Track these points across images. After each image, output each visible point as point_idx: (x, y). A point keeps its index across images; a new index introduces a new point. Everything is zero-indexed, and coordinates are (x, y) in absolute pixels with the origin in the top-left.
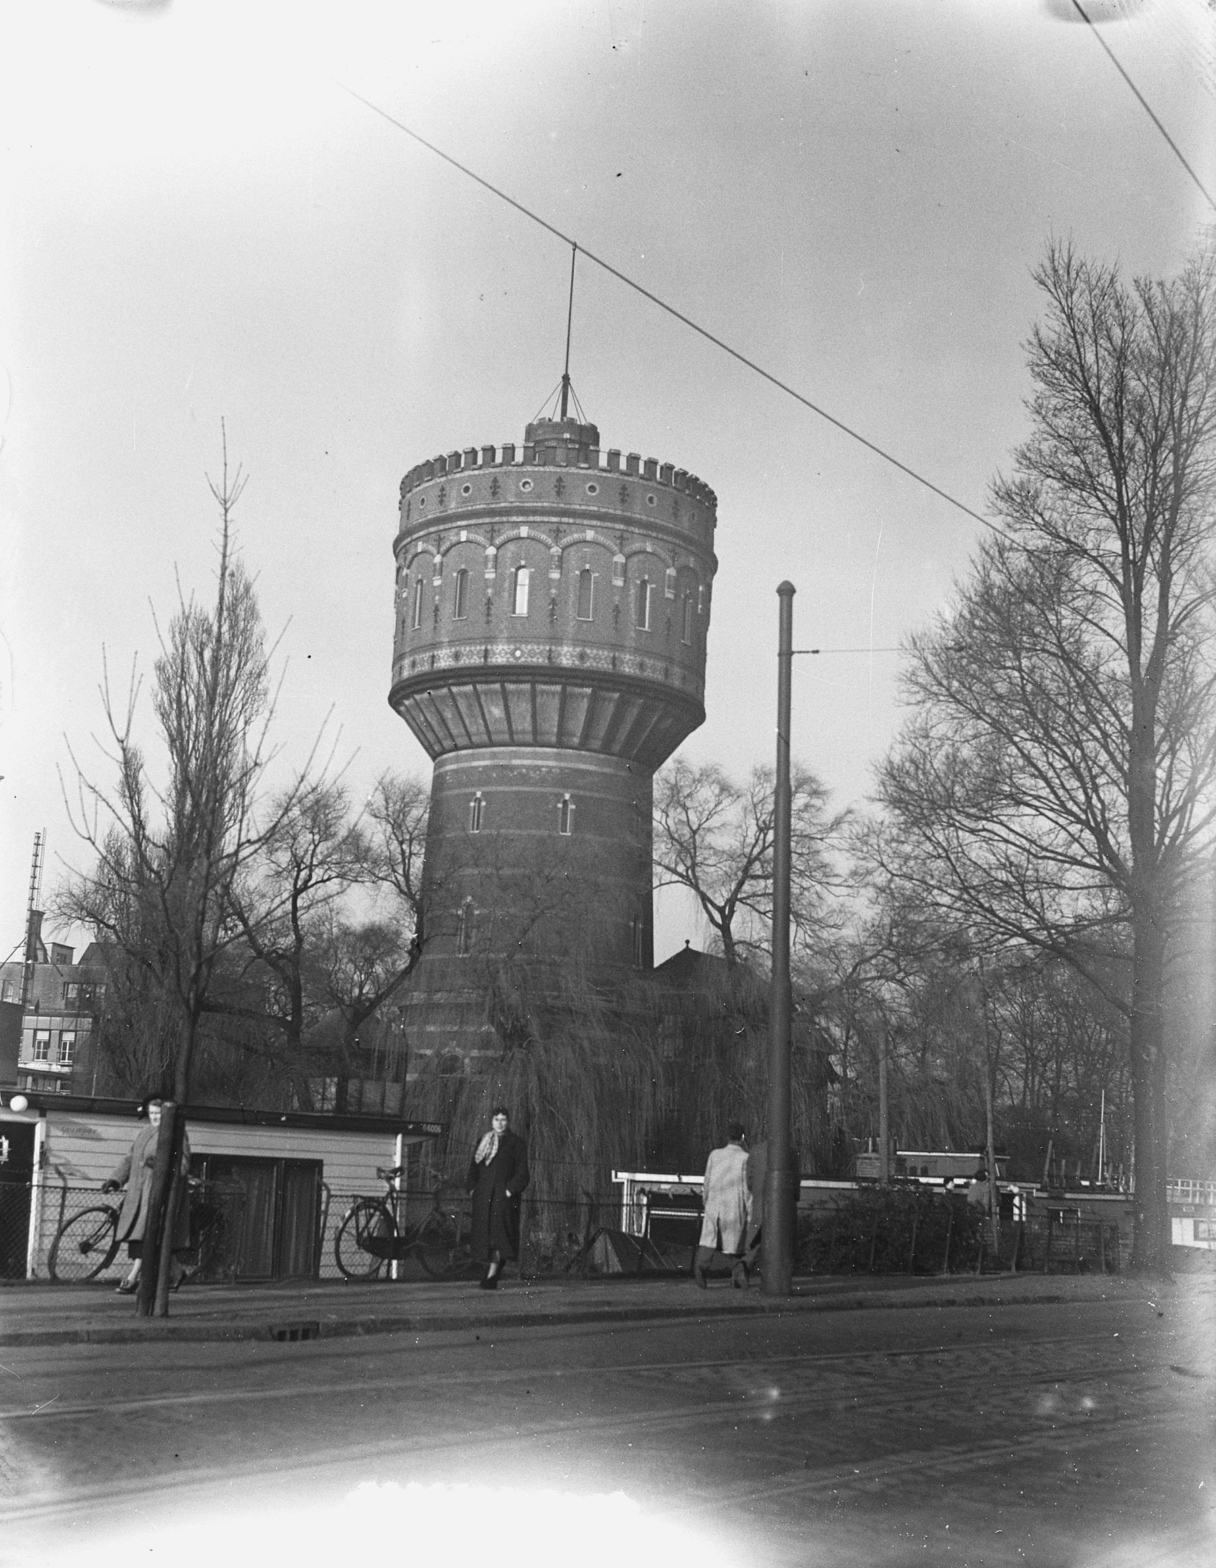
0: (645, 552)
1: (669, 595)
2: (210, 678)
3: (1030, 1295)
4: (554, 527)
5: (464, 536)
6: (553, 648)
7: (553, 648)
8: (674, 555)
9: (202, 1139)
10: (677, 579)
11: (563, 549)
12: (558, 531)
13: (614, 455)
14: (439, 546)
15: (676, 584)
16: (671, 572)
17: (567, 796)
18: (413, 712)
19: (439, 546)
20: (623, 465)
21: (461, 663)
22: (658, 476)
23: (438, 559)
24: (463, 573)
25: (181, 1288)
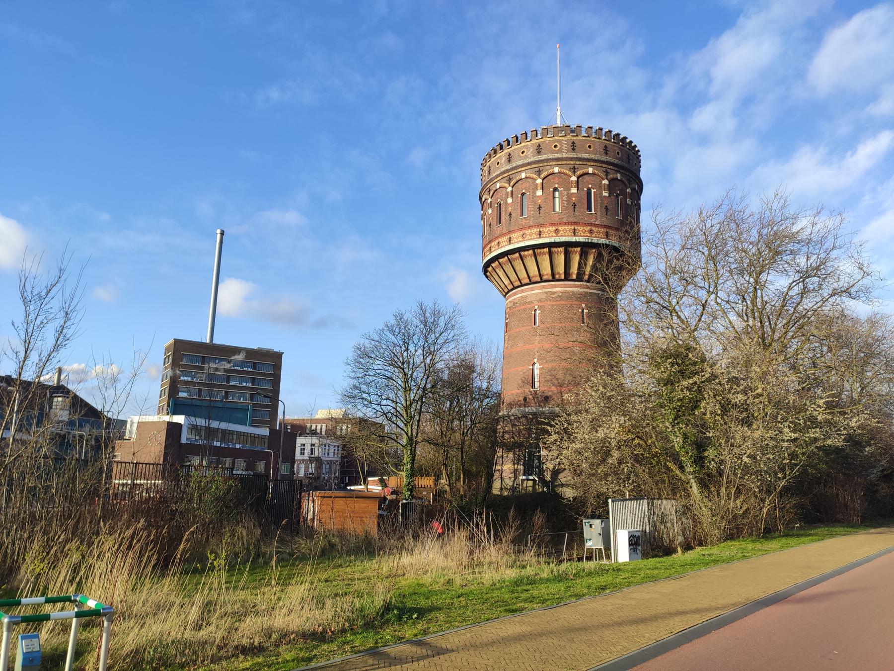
0: (588, 174)
1: (605, 194)
3: (616, 628)
4: (572, 166)
5: (523, 175)
8: (607, 173)
10: (609, 185)
11: (578, 178)
12: (574, 168)
15: (610, 188)
16: (606, 182)
18: (497, 271)
24: (523, 194)
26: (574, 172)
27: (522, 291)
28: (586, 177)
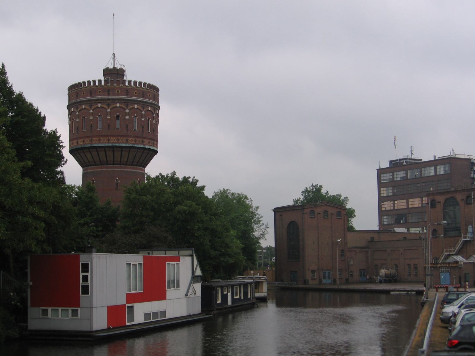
2: (80, 185)
6: (110, 138)
7: (128, 138)
9: (455, 284)
13: (130, 82)
14: (77, 110)
17: (117, 178)
19: (77, 110)
20: (132, 84)
21: (98, 138)
22: (142, 86)
23: (77, 113)
25: (462, 260)
27: (107, 168)
28: (82, 111)
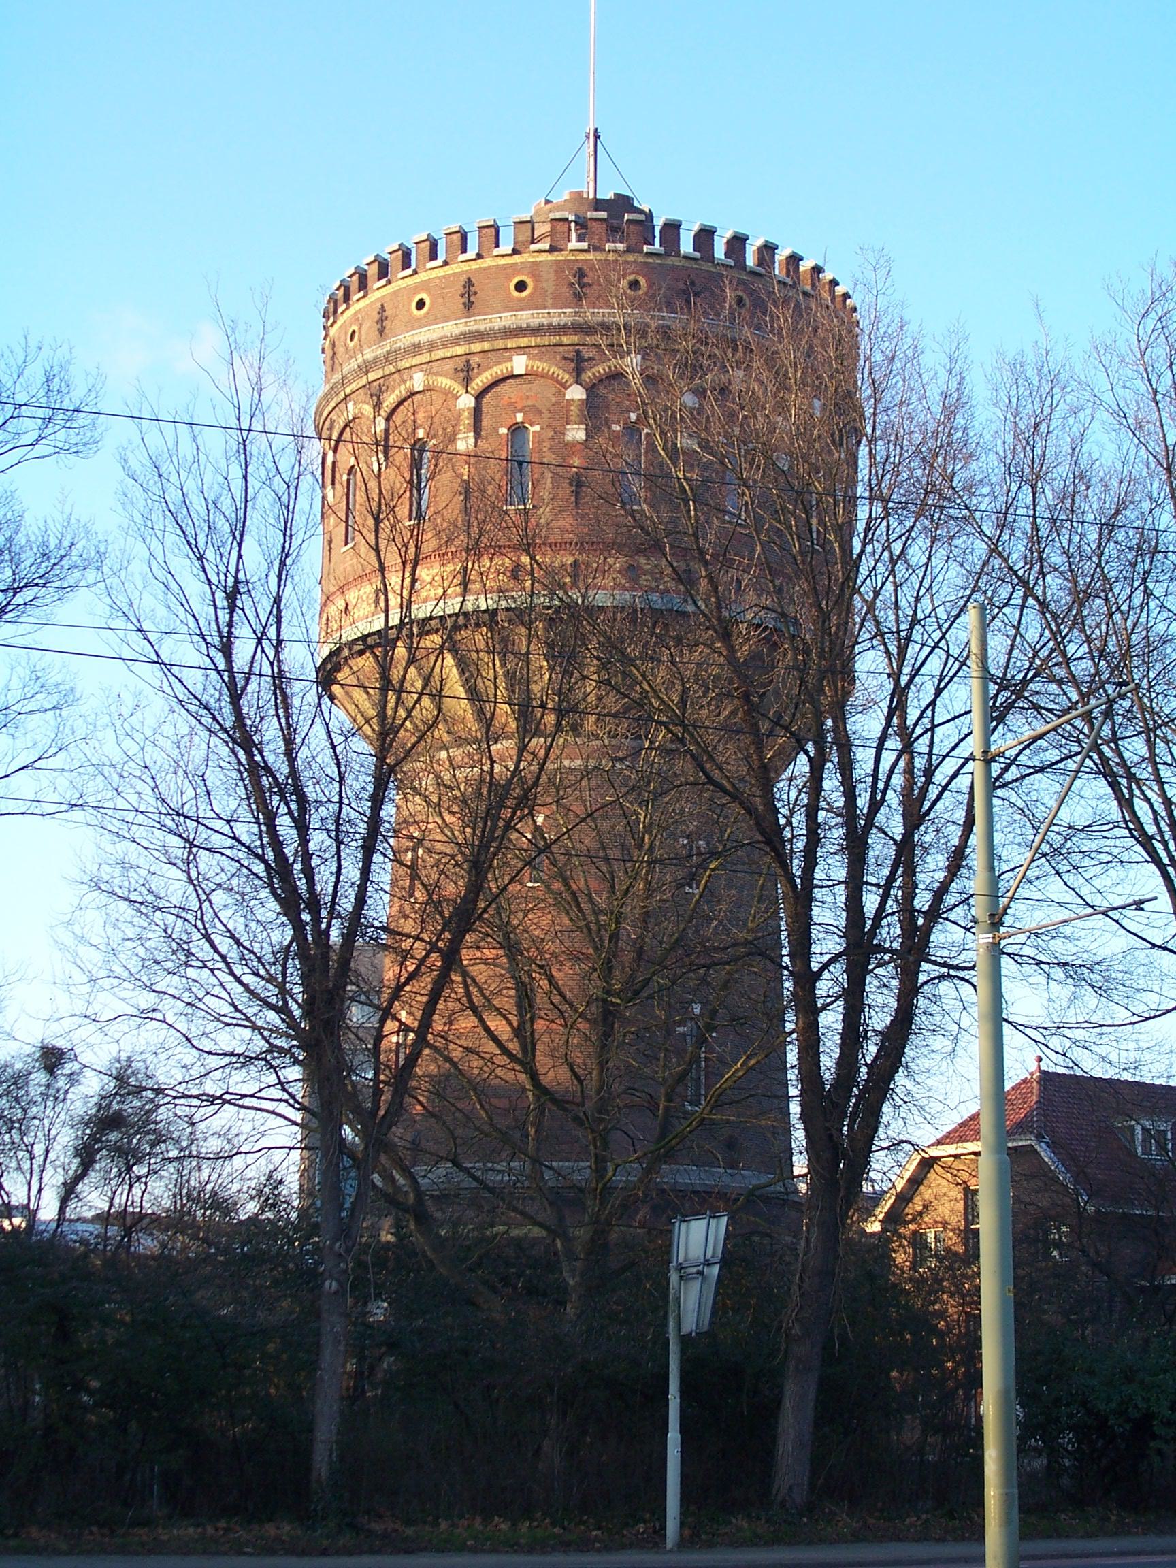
4: (460, 363)
26: (467, 381)
